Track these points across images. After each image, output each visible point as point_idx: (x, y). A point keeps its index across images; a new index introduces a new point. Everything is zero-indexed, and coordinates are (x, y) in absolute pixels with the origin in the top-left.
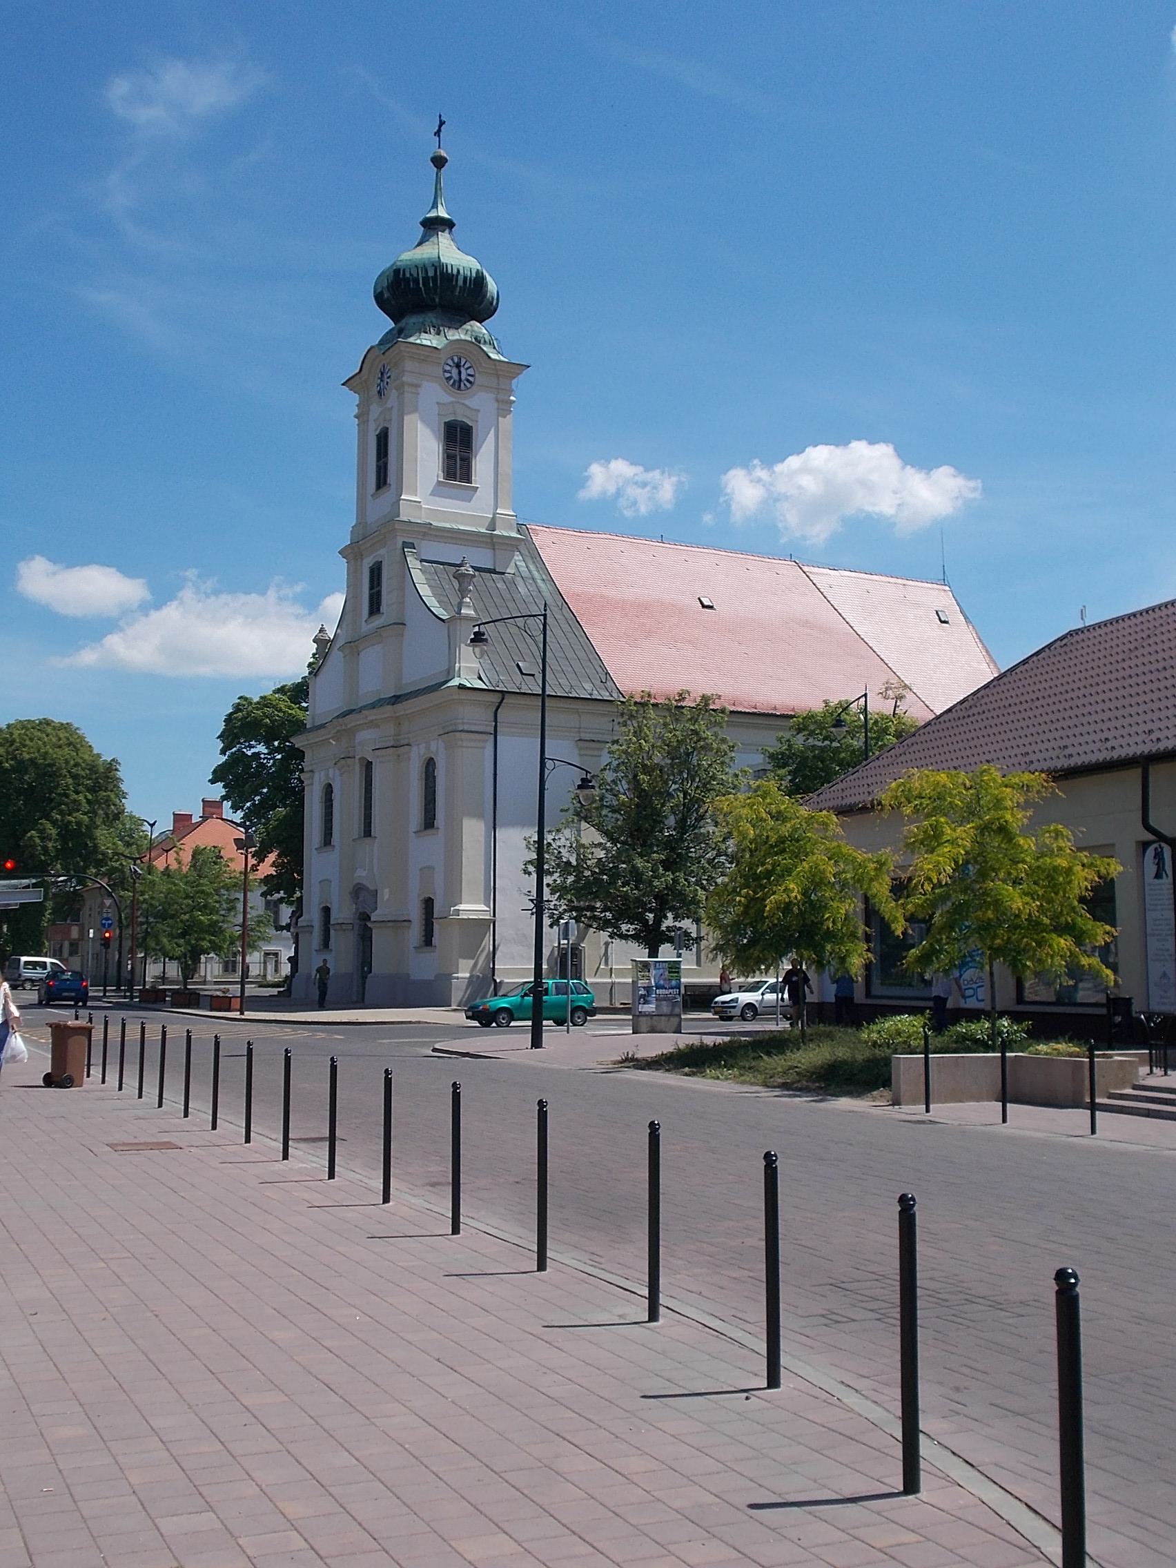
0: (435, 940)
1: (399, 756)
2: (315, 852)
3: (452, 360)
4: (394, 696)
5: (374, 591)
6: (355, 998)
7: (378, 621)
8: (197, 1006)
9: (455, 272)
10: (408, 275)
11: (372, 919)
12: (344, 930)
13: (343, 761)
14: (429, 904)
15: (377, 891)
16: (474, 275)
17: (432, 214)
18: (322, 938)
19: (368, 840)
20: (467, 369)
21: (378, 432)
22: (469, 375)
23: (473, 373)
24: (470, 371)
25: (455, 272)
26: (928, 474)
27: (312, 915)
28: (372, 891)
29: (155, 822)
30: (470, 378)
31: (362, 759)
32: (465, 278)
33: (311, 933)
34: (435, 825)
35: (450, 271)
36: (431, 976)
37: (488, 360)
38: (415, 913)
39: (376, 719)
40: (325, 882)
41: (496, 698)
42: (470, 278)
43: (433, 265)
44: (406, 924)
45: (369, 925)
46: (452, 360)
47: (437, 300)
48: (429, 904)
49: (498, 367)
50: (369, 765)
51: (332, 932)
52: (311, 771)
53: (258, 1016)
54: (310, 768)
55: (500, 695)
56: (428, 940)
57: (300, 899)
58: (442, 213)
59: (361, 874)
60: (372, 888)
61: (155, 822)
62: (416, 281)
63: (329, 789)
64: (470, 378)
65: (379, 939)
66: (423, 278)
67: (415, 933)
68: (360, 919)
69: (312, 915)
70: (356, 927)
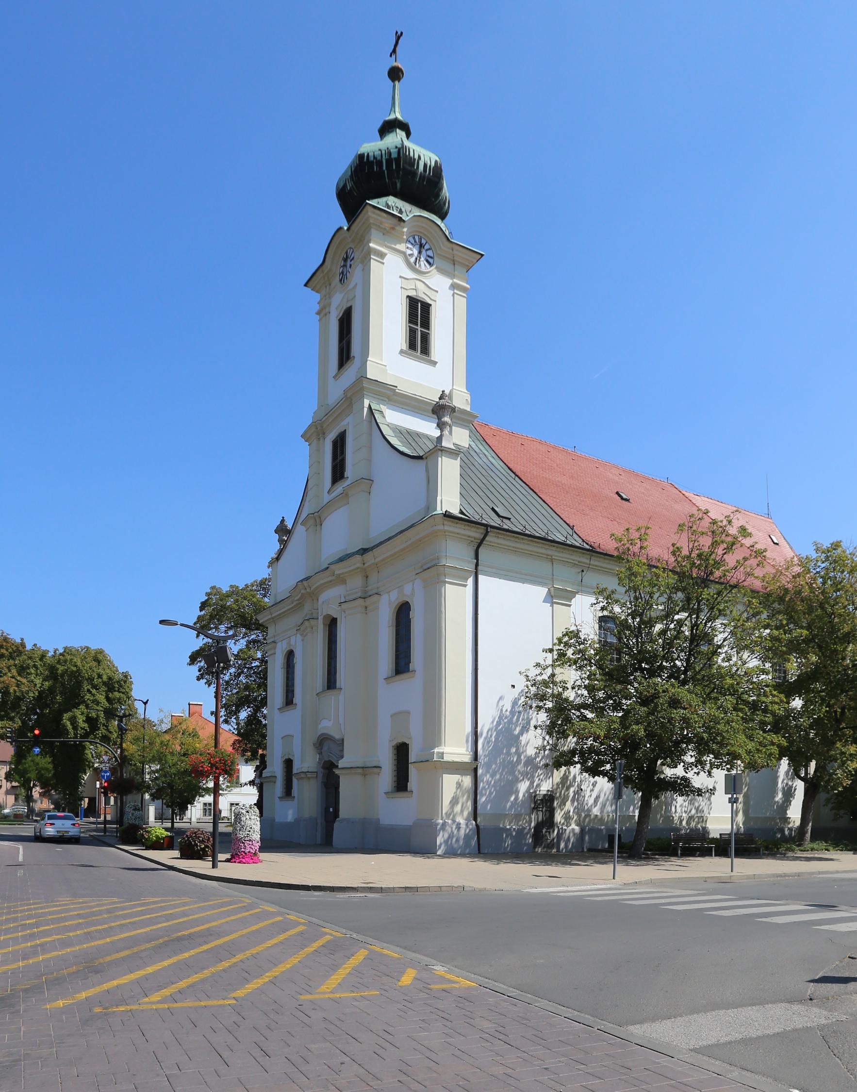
0: (412, 784)
1: (366, 607)
2: (276, 711)
3: (414, 238)
4: (362, 549)
5: (339, 458)
6: (319, 841)
7: (340, 487)
8: (107, 909)
9: (416, 157)
10: (371, 159)
11: (339, 767)
12: (309, 778)
13: (306, 623)
14: (402, 751)
15: (343, 740)
16: (433, 164)
17: (392, 117)
18: (285, 786)
19: (331, 692)
20: (427, 250)
21: (339, 318)
22: (429, 256)
23: (432, 255)
24: (430, 253)
25: (416, 157)
26: (408, 671)
27: (275, 768)
28: (338, 740)
29: (148, 700)
30: (430, 260)
31: (328, 616)
32: (425, 165)
33: (275, 782)
34: (411, 669)
35: (412, 154)
36: (409, 822)
37: (447, 243)
38: (386, 760)
39: (343, 573)
40: (287, 738)
41: (477, 534)
42: (430, 166)
43: (396, 147)
44: (376, 770)
45: (337, 772)
46: (414, 238)
47: (398, 185)
48: (402, 751)
49: (455, 252)
50: (332, 624)
51: (295, 781)
52: (274, 642)
53: (428, 215)
54: (272, 640)
55: (482, 530)
56: (401, 783)
57: (263, 756)
58: (398, 115)
59: (327, 726)
60: (337, 736)
61: (148, 700)
62: (379, 163)
63: (290, 655)
64: (430, 260)
65: (347, 787)
66: (387, 160)
67: (386, 778)
68: (323, 768)
69: (275, 768)
70: (320, 775)
